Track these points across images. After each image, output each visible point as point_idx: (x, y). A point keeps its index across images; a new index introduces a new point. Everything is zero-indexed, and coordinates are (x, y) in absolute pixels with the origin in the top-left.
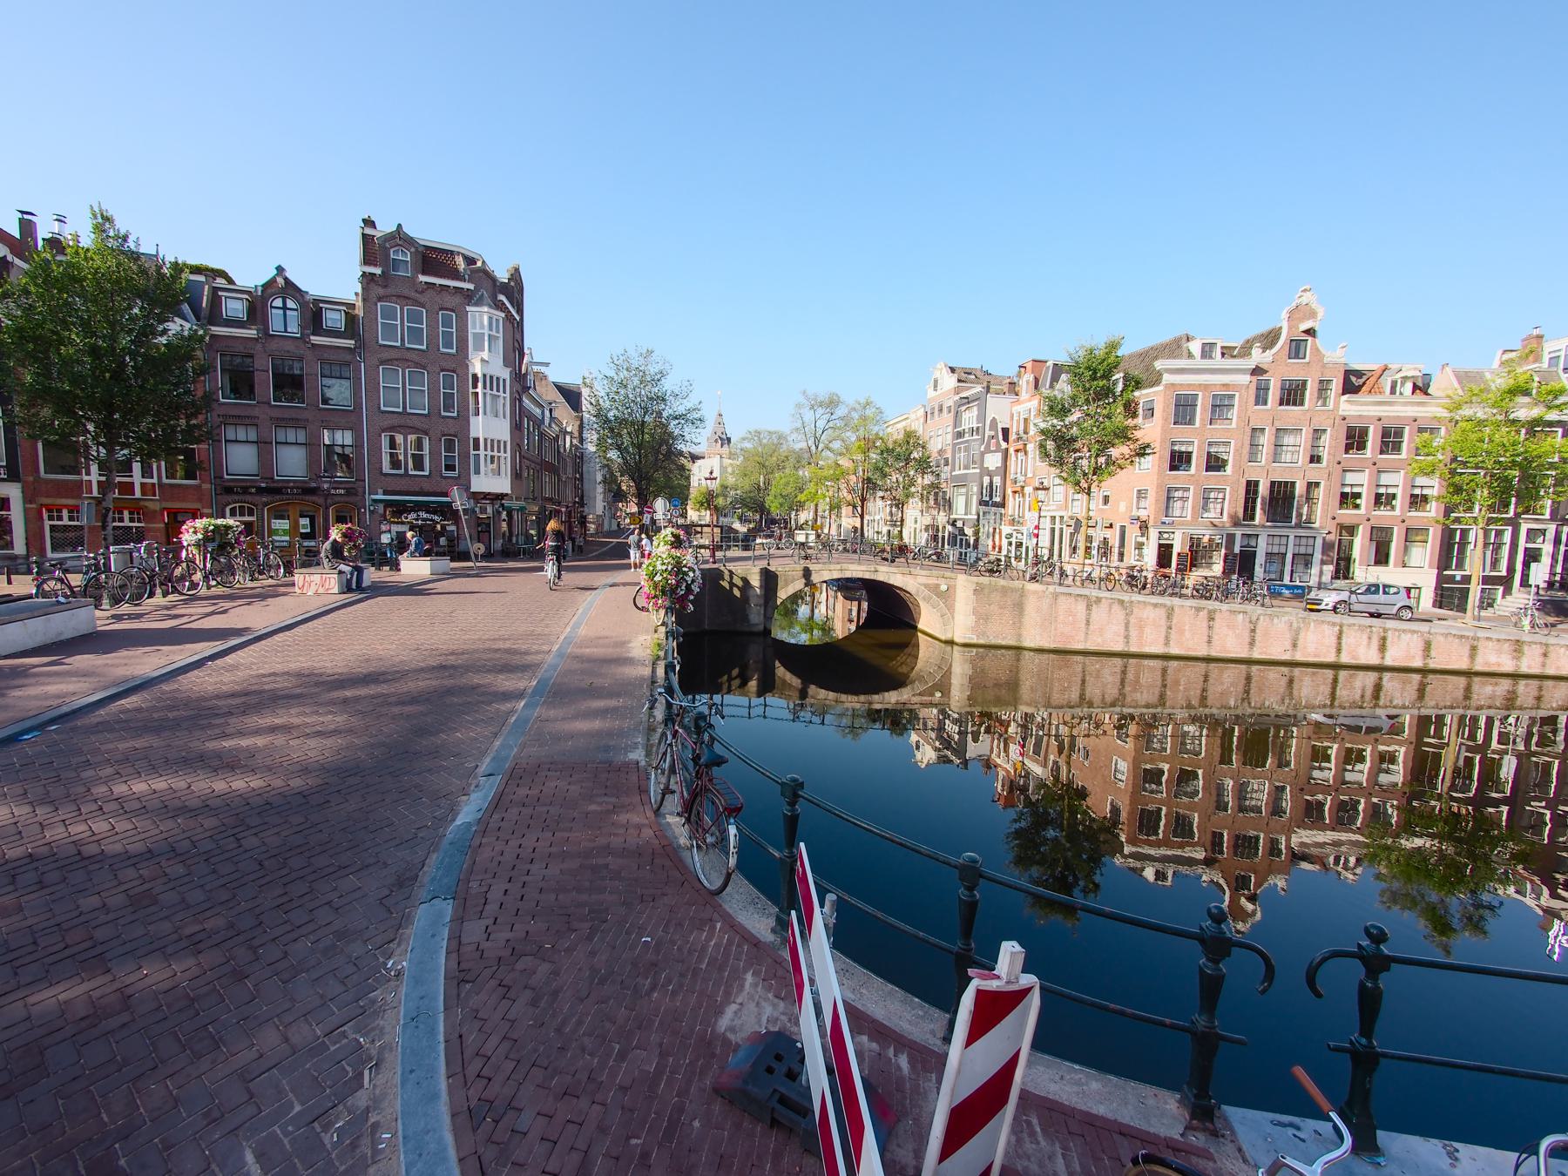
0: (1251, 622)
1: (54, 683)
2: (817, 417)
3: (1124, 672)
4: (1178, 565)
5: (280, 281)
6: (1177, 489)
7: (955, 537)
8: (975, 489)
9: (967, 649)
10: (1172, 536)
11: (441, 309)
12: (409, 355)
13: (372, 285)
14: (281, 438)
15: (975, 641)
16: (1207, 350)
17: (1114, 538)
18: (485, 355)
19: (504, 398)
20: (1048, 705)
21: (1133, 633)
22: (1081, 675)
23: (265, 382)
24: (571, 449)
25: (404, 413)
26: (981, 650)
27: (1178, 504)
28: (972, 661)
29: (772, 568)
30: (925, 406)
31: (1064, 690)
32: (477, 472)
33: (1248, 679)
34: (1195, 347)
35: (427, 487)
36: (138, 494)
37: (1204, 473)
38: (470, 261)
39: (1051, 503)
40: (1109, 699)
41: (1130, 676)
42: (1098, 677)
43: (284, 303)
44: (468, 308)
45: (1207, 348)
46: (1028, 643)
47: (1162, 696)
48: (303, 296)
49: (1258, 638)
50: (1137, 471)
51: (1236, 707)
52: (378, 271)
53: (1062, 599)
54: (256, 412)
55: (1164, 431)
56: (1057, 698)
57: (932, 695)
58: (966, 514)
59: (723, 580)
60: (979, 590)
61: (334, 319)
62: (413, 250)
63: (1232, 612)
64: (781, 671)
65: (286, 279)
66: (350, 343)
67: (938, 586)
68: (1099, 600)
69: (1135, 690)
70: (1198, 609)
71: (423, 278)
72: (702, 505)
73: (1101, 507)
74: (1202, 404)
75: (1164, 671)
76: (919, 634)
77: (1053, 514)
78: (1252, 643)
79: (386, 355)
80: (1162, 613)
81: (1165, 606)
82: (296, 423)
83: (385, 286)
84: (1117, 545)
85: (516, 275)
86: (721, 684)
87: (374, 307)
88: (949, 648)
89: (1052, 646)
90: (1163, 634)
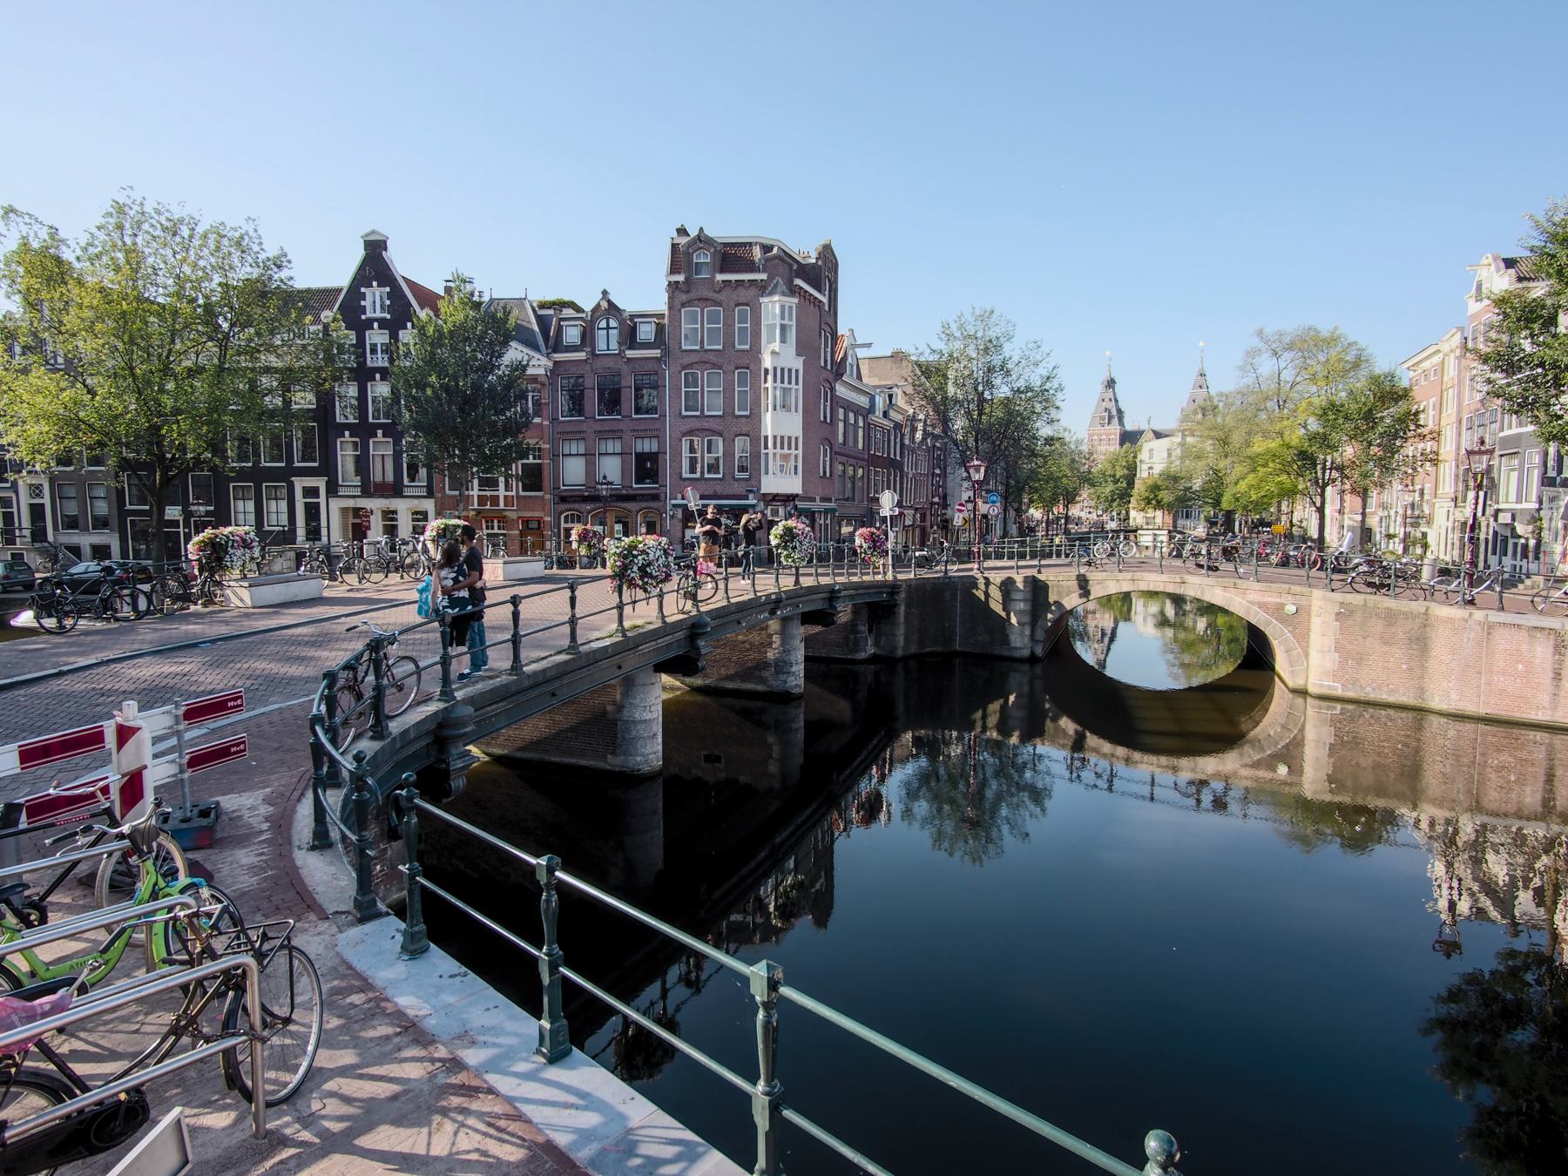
1: (306, 635)
5: (605, 305)
7: (1505, 540)
12: (706, 357)
13: (677, 293)
14: (567, 452)
15: (1339, 692)
18: (776, 346)
19: (797, 390)
20: (1477, 807)
22: (1544, 764)
23: (592, 400)
25: (703, 416)
26: (1350, 707)
28: (1334, 721)
29: (1041, 577)
30: (1461, 329)
32: (767, 473)
35: (720, 489)
36: (502, 505)
38: (767, 248)
43: (608, 323)
44: (762, 300)
46: (1436, 703)
48: (621, 314)
52: (681, 278)
53: (1502, 640)
54: (621, 426)
56: (1492, 798)
57: (1273, 769)
58: (1519, 501)
59: (978, 589)
61: (646, 332)
62: (712, 250)
65: (609, 302)
66: (656, 353)
67: (1281, 606)
71: (720, 277)
72: (1149, 503)
76: (1276, 679)
79: (687, 360)
82: (615, 434)
85: (827, 253)
86: (975, 721)
87: (678, 315)
88: (1300, 701)
89: (1482, 711)
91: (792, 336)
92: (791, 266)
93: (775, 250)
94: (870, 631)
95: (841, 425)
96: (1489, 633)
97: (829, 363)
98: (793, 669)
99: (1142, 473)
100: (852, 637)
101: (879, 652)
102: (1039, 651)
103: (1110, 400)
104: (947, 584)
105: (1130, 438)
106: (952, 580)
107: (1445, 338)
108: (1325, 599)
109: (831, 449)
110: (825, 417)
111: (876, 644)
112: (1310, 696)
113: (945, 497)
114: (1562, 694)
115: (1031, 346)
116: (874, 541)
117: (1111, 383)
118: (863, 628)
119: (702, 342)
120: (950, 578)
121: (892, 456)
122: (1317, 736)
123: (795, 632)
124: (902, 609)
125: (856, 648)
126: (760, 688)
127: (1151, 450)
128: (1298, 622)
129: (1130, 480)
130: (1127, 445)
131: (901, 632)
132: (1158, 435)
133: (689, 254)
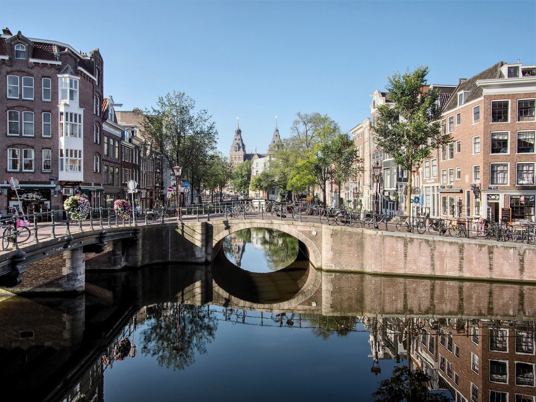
0: (519, 254)
2: (308, 129)
3: (433, 289)
4: (503, 217)
6: (498, 165)
8: (395, 171)
9: (329, 274)
10: (498, 197)
11: (43, 77)
12: (23, 103)
15: (333, 268)
16: (513, 72)
17: (464, 197)
18: (67, 101)
20: (383, 312)
21: (437, 264)
24: (151, 154)
26: (338, 274)
27: (500, 175)
30: (369, 119)
31: (392, 302)
32: (62, 169)
33: (522, 295)
34: (504, 70)
35: (32, 178)
37: (517, 154)
38: (61, 49)
39: (432, 178)
40: (423, 308)
41: (437, 292)
42: (415, 293)
44: (59, 76)
45: (512, 70)
46: (368, 269)
47: (461, 307)
49: (526, 265)
50: (473, 154)
51: (514, 316)
53: (387, 239)
55: (486, 127)
58: (391, 187)
59: (178, 228)
60: (334, 234)
62: (27, 45)
63: (506, 248)
64: (217, 288)
67: (310, 232)
68: (412, 240)
69: (441, 302)
70: (481, 246)
71: (32, 60)
72: (257, 187)
73: (457, 179)
74: (511, 108)
75: (461, 288)
77: (433, 185)
78: (522, 270)
79: (10, 104)
80: (456, 248)
81: (457, 244)
83: (11, 66)
84: (466, 204)
85: (96, 54)
86: (177, 298)
88: (319, 273)
89: (383, 271)
90: (458, 263)
91: (77, 96)
92: (76, 60)
93: (66, 50)
94: (123, 254)
95: (106, 145)
96: (383, 240)
97: (98, 112)
98: (79, 277)
99: (254, 173)
100: (113, 258)
101: (128, 265)
102: (209, 258)
103: (239, 139)
104: (164, 227)
105: (248, 157)
106: (166, 225)
107: (364, 122)
108: (327, 228)
109: (100, 158)
110: (97, 141)
111: (126, 260)
112: (323, 271)
113: (162, 184)
114: (407, 262)
115: (203, 112)
116: (124, 207)
117: (239, 132)
118: (119, 252)
119: (21, 95)
120: (165, 224)
121: (134, 163)
122: (326, 287)
123: (79, 257)
124: (140, 242)
125: (115, 263)
126: (57, 290)
127: (257, 163)
128: (317, 238)
129: (249, 176)
130: (247, 160)
131: (140, 254)
132: (260, 156)
133: (11, 45)
